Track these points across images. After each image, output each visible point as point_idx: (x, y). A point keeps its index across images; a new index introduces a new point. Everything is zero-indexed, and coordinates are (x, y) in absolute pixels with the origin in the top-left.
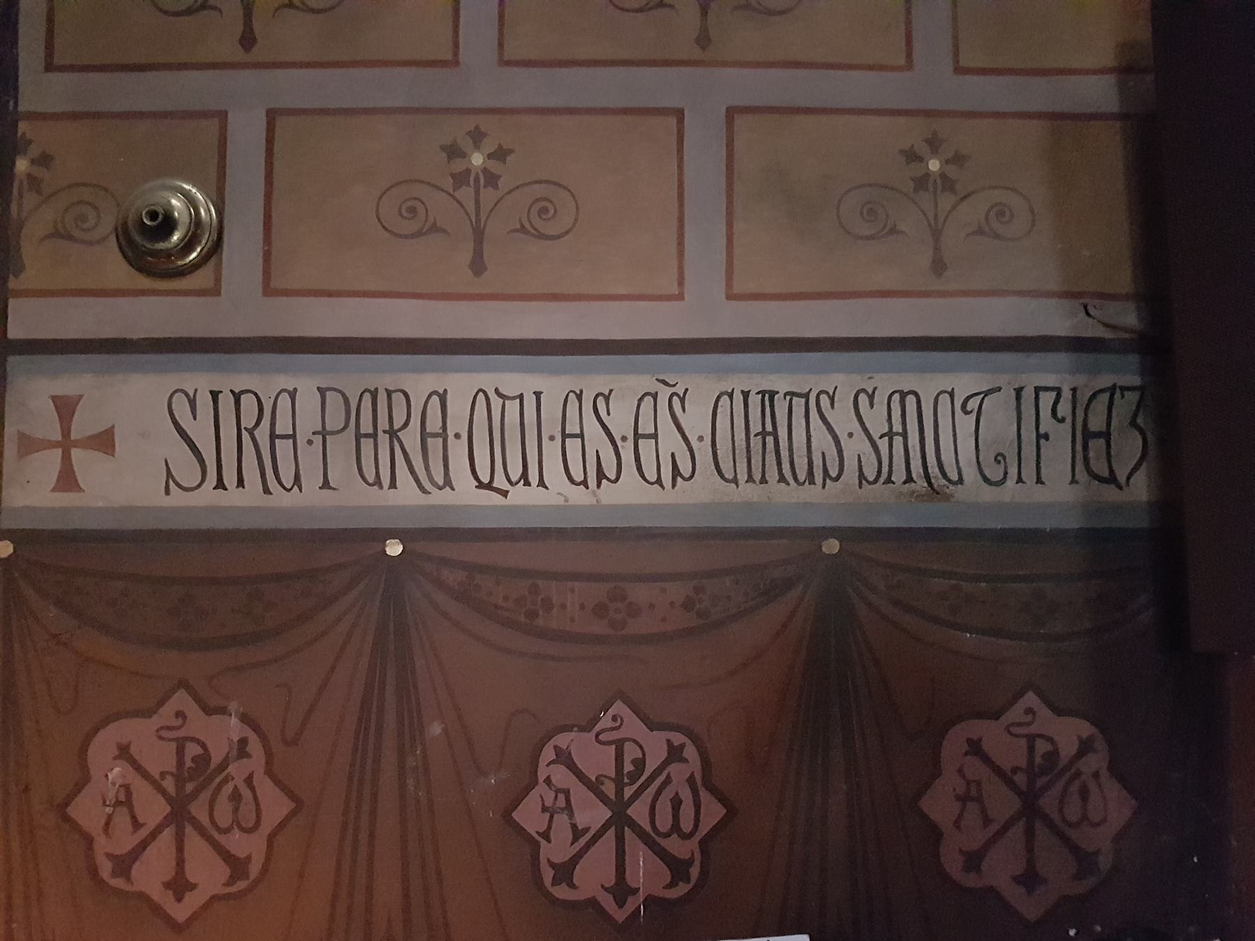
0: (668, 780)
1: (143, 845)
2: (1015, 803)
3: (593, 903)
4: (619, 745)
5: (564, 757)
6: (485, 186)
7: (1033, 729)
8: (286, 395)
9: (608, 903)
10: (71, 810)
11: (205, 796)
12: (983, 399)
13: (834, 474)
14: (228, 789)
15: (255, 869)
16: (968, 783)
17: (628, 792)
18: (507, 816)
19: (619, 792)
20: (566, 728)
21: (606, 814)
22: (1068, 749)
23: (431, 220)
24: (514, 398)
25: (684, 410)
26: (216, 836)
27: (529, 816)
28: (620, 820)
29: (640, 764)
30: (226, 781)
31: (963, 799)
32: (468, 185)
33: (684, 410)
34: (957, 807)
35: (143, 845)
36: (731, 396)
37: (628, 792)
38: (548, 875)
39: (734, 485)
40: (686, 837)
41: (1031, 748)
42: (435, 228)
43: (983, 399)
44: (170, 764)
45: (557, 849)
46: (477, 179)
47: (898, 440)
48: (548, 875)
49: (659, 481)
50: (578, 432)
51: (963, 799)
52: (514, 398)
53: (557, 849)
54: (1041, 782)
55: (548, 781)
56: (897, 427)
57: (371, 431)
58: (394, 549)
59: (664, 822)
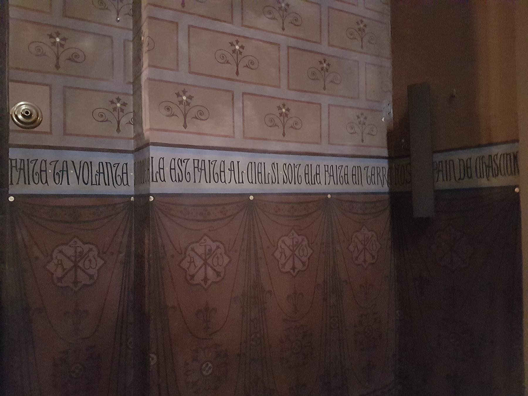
0: (216, 254)
1: (198, 271)
2: (202, 262)
3: (288, 272)
4: (293, 239)
5: (61, 252)
6: (186, 106)
7: (205, 244)
8: (162, 159)
9: (292, 271)
10: (181, 265)
11: (82, 261)
12: (56, 163)
13: (274, 182)
14: (302, 248)
15: (222, 275)
16: (282, 249)
17: (366, 243)
18: (273, 255)
19: (364, 243)
20: (193, 243)
21: (202, 262)
22: (214, 248)
23: (173, 113)
24: (14, 160)
25: (182, 166)
26: (214, 267)
27: (51, 267)
28: (206, 263)
29: (297, 242)
30: (216, 254)
31: (281, 253)
32: (282, 116)
33: (182, 166)
34: (188, 264)
35: (198, 271)
36: (251, 163)
37: (78, 260)
38: (281, 266)
39: (252, 184)
40: (306, 256)
41: (205, 248)
42: (276, 125)
43: (56, 163)
44: (291, 244)
45: (282, 261)
46: (185, 104)
47: (102, 175)
48: (188, 278)
49: (252, 182)
50: (45, 170)
51: (190, 262)
52: (14, 160)
53: (282, 261)
54: (208, 257)
55: (189, 255)
56: (101, 171)
57: (174, 168)
58: (251, 198)
59: (215, 264)
